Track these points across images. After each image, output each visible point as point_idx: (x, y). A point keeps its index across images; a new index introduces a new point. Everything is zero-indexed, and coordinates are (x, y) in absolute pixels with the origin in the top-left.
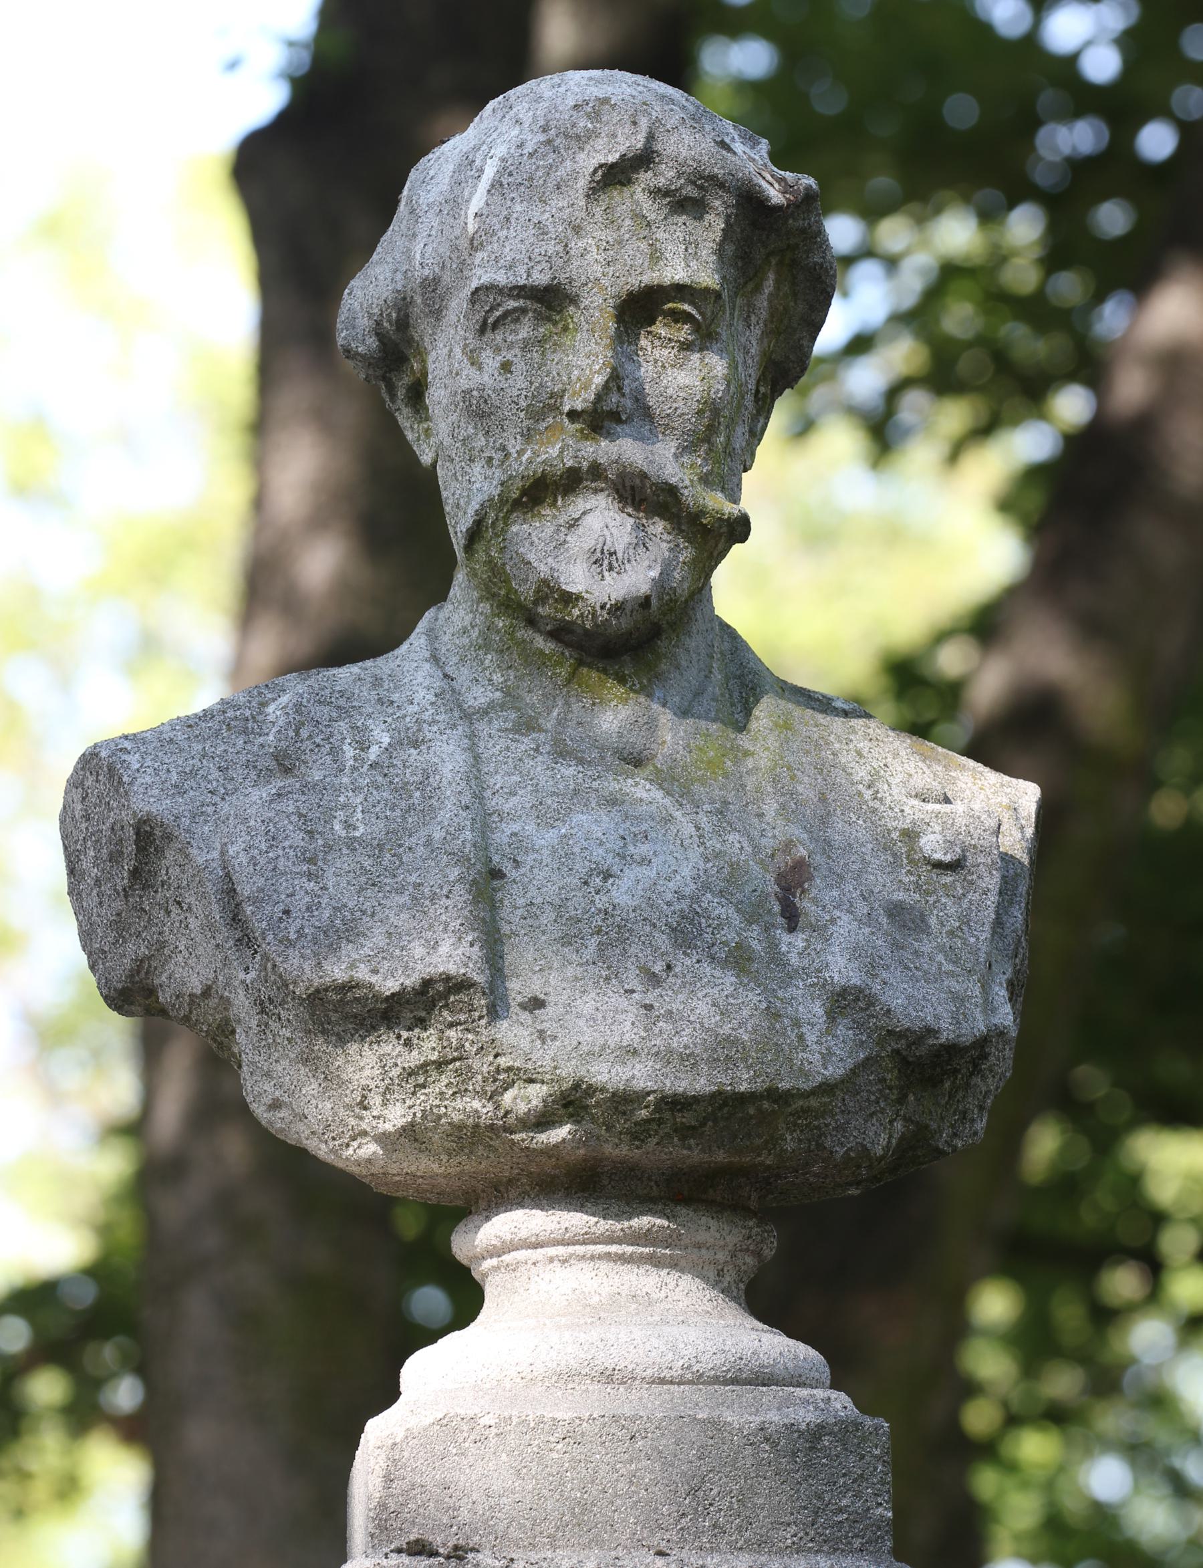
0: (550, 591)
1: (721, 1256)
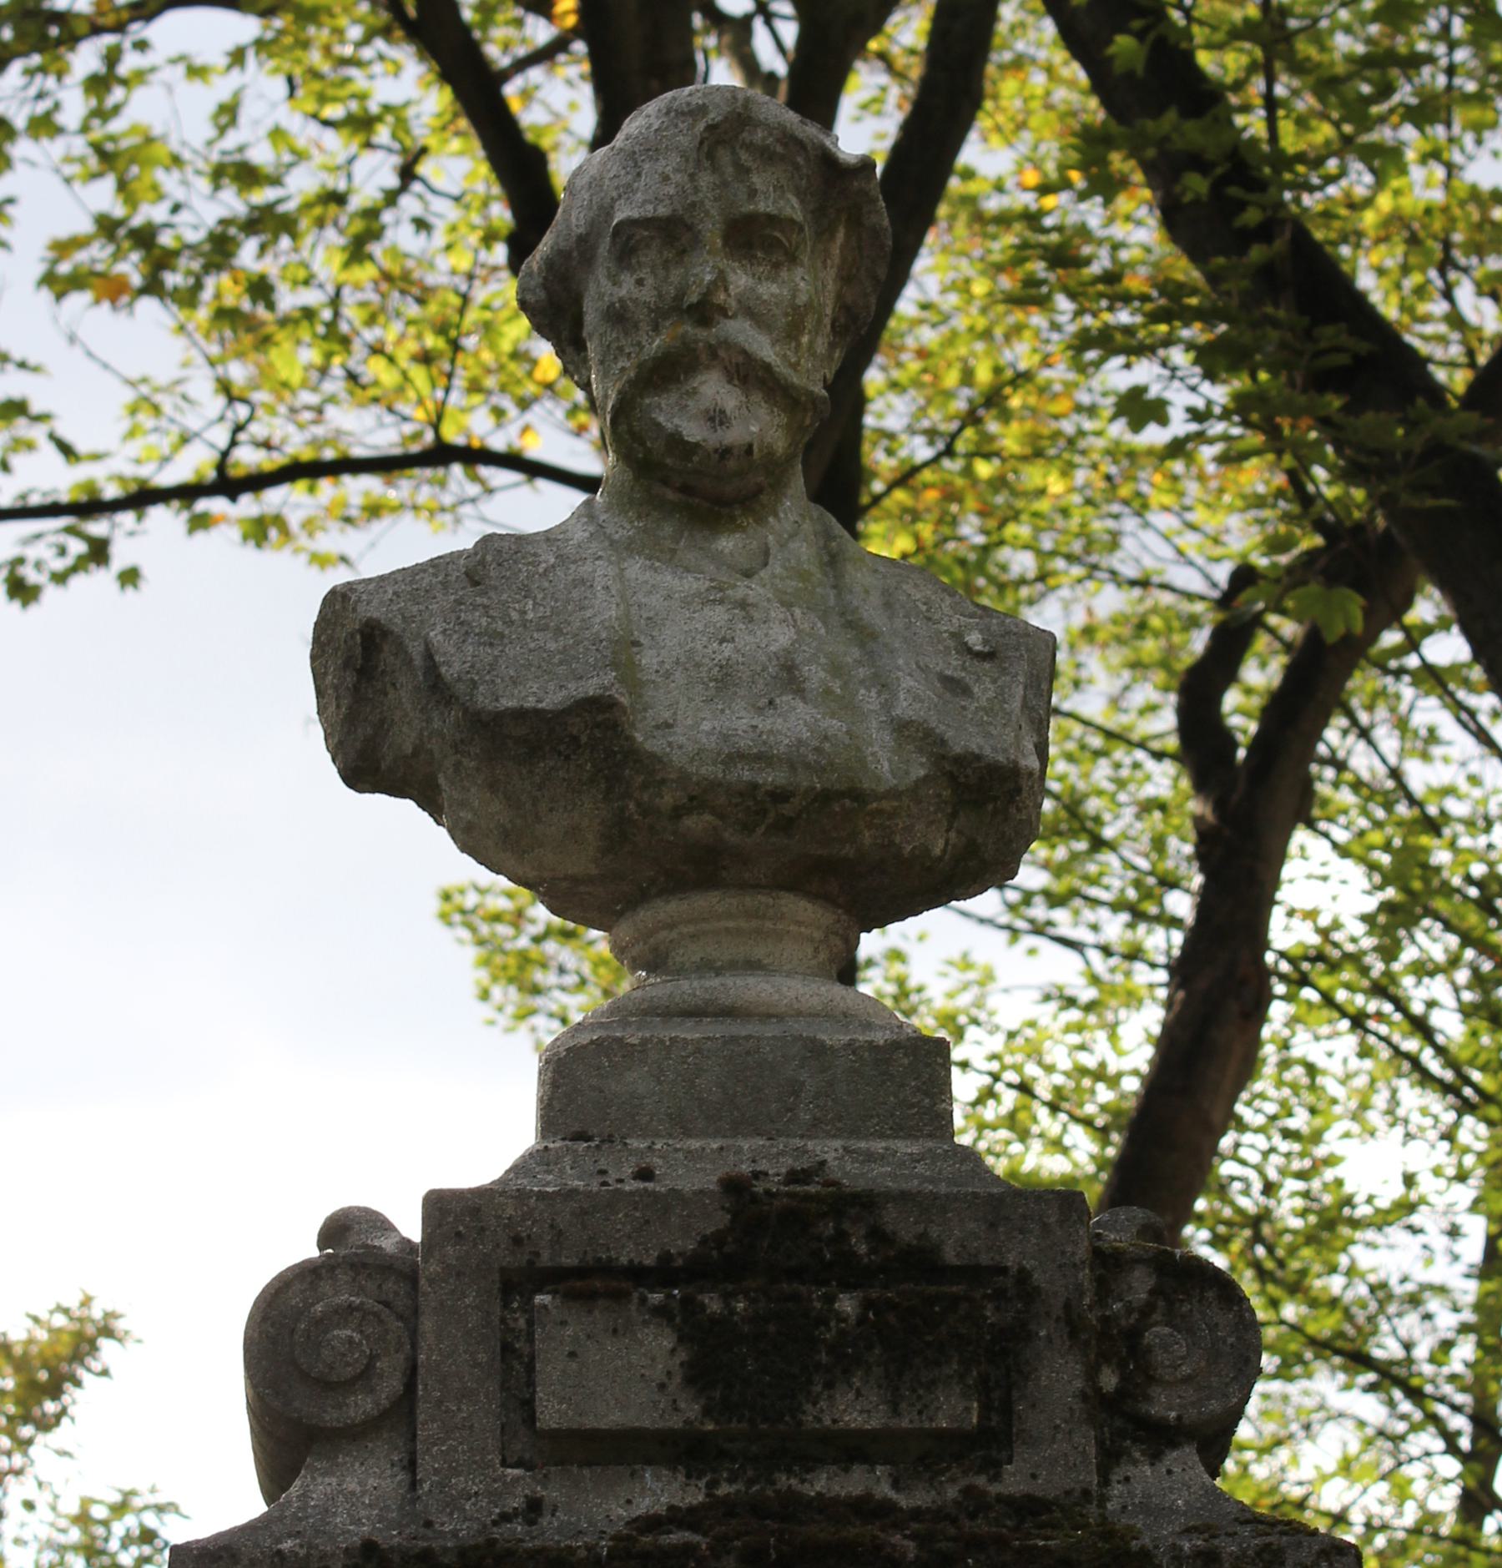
0: (676, 442)
1: (818, 935)
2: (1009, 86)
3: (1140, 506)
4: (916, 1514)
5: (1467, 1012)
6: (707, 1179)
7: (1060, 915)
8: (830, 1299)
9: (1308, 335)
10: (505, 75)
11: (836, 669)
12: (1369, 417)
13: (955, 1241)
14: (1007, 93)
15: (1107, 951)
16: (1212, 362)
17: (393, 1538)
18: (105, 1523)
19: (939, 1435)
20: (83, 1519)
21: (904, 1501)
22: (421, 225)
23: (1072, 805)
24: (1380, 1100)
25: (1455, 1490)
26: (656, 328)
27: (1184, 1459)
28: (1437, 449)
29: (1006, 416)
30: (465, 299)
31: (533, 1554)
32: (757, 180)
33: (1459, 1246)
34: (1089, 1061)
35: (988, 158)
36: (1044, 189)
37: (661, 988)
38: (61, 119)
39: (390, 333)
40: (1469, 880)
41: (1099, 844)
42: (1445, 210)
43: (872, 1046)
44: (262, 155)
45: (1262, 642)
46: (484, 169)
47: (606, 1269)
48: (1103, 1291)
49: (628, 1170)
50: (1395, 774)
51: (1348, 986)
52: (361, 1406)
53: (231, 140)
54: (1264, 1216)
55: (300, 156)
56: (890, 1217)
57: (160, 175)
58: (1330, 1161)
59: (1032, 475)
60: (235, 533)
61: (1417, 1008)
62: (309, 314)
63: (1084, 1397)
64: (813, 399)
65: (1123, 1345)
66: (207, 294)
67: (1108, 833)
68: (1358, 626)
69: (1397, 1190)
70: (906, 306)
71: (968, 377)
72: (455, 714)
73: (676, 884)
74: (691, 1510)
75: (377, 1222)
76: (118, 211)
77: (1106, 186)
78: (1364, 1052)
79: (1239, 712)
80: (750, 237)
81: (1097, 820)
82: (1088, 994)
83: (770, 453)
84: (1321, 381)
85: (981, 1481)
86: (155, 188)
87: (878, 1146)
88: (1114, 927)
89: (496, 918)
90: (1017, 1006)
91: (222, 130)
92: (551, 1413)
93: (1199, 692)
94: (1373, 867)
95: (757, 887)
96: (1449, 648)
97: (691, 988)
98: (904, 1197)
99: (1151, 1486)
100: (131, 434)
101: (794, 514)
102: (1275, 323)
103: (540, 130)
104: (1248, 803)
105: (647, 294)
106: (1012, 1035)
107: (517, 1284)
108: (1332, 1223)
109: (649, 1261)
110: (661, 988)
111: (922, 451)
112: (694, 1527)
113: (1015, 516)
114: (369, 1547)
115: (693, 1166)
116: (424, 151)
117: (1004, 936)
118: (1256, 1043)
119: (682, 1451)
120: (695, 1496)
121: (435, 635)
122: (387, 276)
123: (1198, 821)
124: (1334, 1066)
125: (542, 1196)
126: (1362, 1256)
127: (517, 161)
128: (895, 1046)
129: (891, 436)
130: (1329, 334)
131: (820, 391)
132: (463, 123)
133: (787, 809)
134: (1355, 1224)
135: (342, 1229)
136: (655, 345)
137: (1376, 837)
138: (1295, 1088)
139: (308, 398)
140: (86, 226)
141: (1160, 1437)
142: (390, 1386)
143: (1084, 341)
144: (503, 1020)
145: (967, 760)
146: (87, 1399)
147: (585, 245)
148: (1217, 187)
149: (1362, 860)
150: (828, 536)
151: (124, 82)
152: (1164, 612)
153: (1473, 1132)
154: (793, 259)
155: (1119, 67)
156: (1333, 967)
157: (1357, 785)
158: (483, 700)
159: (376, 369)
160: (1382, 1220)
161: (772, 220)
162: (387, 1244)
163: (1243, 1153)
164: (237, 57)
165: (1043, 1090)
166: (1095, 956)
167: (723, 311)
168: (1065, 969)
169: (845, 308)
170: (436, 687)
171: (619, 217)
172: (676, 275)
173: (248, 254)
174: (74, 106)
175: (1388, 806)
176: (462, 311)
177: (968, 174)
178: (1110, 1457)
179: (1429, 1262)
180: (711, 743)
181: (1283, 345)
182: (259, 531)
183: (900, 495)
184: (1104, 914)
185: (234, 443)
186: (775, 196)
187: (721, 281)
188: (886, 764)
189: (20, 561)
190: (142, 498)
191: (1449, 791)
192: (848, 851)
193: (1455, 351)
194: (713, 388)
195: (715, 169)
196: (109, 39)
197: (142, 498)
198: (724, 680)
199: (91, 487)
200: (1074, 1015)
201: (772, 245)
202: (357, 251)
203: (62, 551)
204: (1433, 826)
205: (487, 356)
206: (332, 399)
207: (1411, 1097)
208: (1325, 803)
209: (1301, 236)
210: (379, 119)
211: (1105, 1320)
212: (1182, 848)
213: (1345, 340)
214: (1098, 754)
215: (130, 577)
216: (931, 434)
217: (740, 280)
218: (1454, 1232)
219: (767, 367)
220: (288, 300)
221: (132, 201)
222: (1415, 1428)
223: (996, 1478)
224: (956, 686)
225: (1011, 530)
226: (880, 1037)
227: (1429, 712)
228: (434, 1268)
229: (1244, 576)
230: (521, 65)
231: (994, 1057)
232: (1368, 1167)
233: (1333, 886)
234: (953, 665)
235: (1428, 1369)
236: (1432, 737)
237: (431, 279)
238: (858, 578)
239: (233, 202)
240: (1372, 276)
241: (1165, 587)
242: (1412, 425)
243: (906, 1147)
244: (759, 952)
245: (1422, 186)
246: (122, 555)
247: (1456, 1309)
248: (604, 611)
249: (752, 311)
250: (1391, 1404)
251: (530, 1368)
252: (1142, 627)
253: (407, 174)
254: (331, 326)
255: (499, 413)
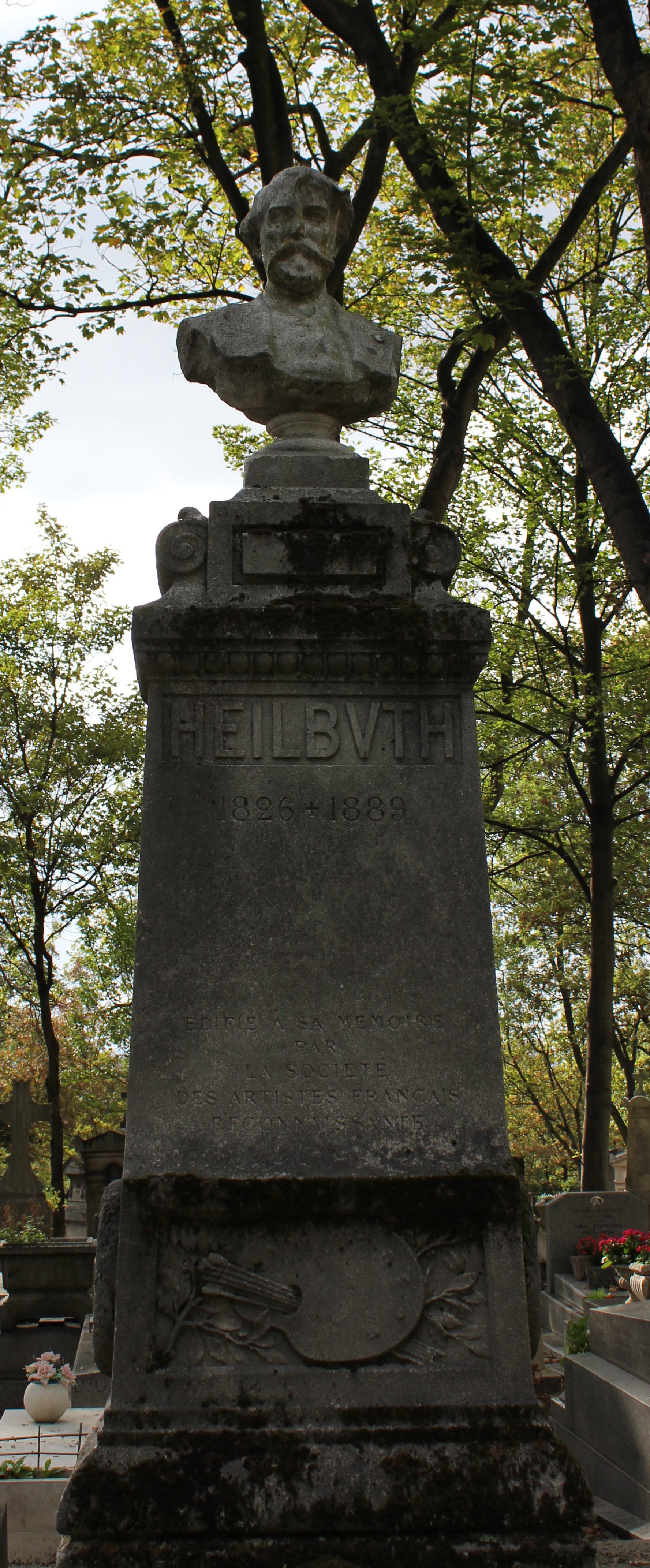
0: (288, 275)
2: (389, 182)
3: (427, 313)
4: (357, 600)
5: (522, 467)
6: (295, 499)
7: (401, 437)
8: (332, 535)
9: (480, 257)
10: (236, 177)
11: (336, 345)
12: (498, 282)
13: (370, 518)
14: (389, 184)
15: (415, 448)
16: (450, 265)
17: (200, 605)
18: (112, 617)
19: (364, 576)
20: (105, 615)
21: (353, 596)
22: (209, 222)
23: (405, 403)
24: (496, 494)
25: (516, 611)
26: (282, 241)
27: (437, 585)
28: (518, 292)
29: (387, 283)
30: (223, 245)
31: (242, 610)
32: (313, 196)
33: (519, 538)
34: (409, 481)
35: (381, 205)
36: (400, 211)
37: (282, 442)
38: (100, 189)
39: (199, 256)
40: (525, 427)
41: (413, 415)
42: (522, 221)
43: (345, 460)
44: (161, 201)
45: (464, 354)
46: (228, 205)
47: (264, 526)
48: (414, 534)
49: (271, 496)
50: (503, 395)
51: (487, 459)
52: (190, 566)
53: (152, 196)
54: (462, 528)
55: (173, 201)
56: (350, 511)
57: (130, 207)
58: (481, 512)
59: (395, 302)
60: (152, 317)
61: (508, 466)
62: (175, 249)
63: (408, 566)
64: (330, 263)
65: (419, 550)
66: (144, 244)
67: (416, 412)
68: (493, 346)
69: (501, 521)
70: (356, 250)
71: (375, 269)
72: (220, 358)
73: (287, 411)
74: (290, 598)
75: (194, 511)
76: (117, 218)
77: (418, 211)
78: (492, 480)
79: (456, 374)
80: (311, 213)
81: (413, 408)
82: (408, 461)
83: (316, 279)
84: (484, 271)
85: (376, 590)
86: (128, 211)
87: (347, 490)
88: (417, 441)
89: (231, 436)
90: (388, 455)
91: (149, 193)
92: (248, 569)
93: (444, 368)
94: (495, 423)
95: (311, 411)
96: (521, 355)
97: (291, 442)
98: (355, 505)
99: (428, 593)
100: (121, 286)
101: (323, 299)
102: (469, 253)
103: (246, 194)
104: (459, 401)
105: (279, 230)
106: (386, 473)
107: (238, 530)
108: (482, 529)
109: (277, 523)
110: (282, 442)
111: (360, 293)
112: (290, 603)
113: (389, 315)
114: (193, 608)
115: (291, 495)
116: (211, 200)
117: (384, 443)
118: (459, 476)
119: (286, 580)
120: (291, 594)
121: (214, 334)
122: (199, 238)
123: (443, 406)
124: (483, 484)
125: (245, 503)
126: (491, 541)
127: (238, 203)
128: (352, 460)
129: (352, 289)
130: (486, 256)
131: (332, 260)
132: (222, 191)
133: (320, 388)
134: (489, 531)
135: (187, 514)
136: (282, 246)
137: (497, 414)
138: (470, 489)
139: (174, 276)
140: (108, 223)
141: (430, 578)
142: (199, 560)
143: (411, 258)
144: (232, 467)
145: (376, 373)
146: (108, 580)
147: (261, 215)
148: (452, 211)
149: (492, 421)
150: (334, 305)
151: (119, 178)
152: (434, 345)
153: (524, 504)
154: (324, 220)
155: (423, 174)
156: (483, 454)
157: (491, 398)
158: (228, 354)
159: (196, 267)
160: (496, 530)
161: (318, 208)
162: (198, 518)
163: (456, 509)
164: (154, 170)
165: (395, 489)
166: (411, 449)
167: (302, 236)
168: (402, 453)
169: (340, 236)
170: (214, 349)
171: (271, 206)
172: (288, 224)
173: (156, 231)
174: (104, 186)
175: (501, 406)
176: (222, 249)
177: (376, 210)
178: (415, 584)
179: (510, 543)
180: (297, 367)
181: (472, 260)
182: (161, 316)
183: (354, 307)
184: (414, 436)
185: (152, 289)
186: (319, 201)
187: (302, 226)
188: (351, 374)
189: (87, 325)
190: (124, 306)
191: (520, 400)
192: (339, 401)
193: (524, 265)
194: (299, 259)
195: (301, 192)
196: (115, 164)
197: (124, 306)
198: (302, 348)
199: (109, 302)
200: (405, 467)
201: (318, 216)
202: (190, 230)
203: (100, 322)
204: (514, 411)
205: (229, 263)
206: (182, 276)
207: (506, 493)
208: (482, 403)
209: (479, 226)
210: (197, 190)
211: (414, 543)
212: (438, 417)
213: (491, 258)
214: (413, 388)
215: (120, 330)
216: (364, 289)
217: (308, 226)
218: (518, 534)
219: (316, 253)
220: (169, 246)
221: (122, 215)
222: (504, 593)
223: (381, 589)
224: (372, 351)
225: (388, 319)
226: (348, 457)
227: (514, 377)
228: (213, 525)
229: (458, 332)
230: (240, 174)
231: (381, 479)
232: (493, 514)
233: (483, 429)
234: (371, 345)
235: (509, 575)
236: (515, 383)
237: (212, 240)
238: (343, 317)
239: (152, 215)
240: (499, 240)
241: (434, 337)
242: (511, 284)
243: (355, 490)
244: (311, 431)
245: (514, 213)
246: (118, 323)
247: (518, 557)
248: (266, 327)
249: (311, 236)
250: (498, 585)
251: (241, 555)
252: (427, 349)
253: (205, 207)
254: (182, 253)
255: (232, 281)
